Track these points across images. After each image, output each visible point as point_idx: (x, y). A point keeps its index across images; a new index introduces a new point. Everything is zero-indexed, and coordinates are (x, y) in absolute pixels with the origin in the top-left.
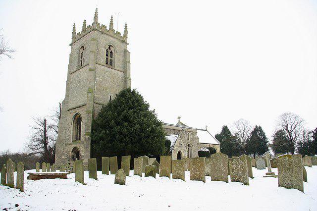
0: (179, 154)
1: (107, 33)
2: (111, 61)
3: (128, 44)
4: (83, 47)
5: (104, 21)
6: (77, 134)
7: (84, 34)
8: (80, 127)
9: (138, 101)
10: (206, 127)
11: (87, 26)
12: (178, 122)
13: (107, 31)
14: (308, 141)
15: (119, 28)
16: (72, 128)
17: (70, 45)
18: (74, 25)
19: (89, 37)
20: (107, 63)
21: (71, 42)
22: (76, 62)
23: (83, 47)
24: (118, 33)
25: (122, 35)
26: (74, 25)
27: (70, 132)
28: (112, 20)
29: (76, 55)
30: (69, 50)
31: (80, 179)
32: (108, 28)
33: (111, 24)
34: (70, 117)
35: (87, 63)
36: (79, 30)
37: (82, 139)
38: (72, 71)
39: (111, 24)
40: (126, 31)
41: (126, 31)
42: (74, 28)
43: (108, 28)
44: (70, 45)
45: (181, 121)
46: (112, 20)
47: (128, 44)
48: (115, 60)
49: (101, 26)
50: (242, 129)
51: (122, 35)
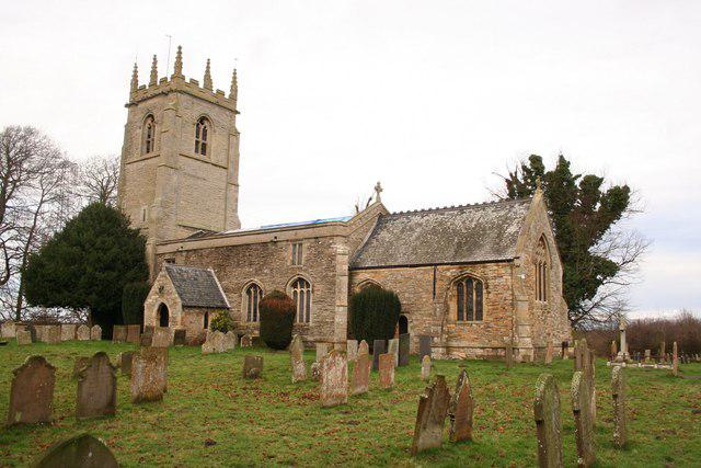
0: (163, 310)
2: (204, 145)
3: (237, 112)
4: (151, 116)
5: (193, 72)
10: (378, 189)
11: (159, 78)
14: (56, 233)
15: (221, 84)
17: (127, 106)
19: (170, 102)
20: (196, 151)
22: (139, 141)
30: (123, 115)
31: (563, 165)
32: (201, 86)
36: (144, 80)
39: (208, 77)
41: (234, 88)
44: (127, 106)
50: (426, 209)
51: (227, 96)
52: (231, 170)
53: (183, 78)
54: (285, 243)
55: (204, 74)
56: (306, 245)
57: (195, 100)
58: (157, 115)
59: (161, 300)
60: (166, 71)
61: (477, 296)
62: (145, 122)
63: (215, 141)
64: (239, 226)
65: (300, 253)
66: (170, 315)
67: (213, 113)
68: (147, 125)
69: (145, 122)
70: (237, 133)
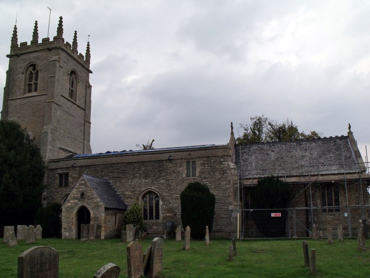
44: (8, 56)
52: (87, 111)
53: (63, 40)
54: (180, 161)
55: (73, 38)
56: (198, 162)
57: (69, 58)
58: (40, 66)
59: (80, 204)
60: (52, 35)
61: (335, 196)
62: (27, 70)
63: (80, 90)
64: (91, 152)
65: (194, 169)
66: (92, 215)
67: (79, 69)
68: (28, 72)
69: (27, 70)
70: (90, 87)
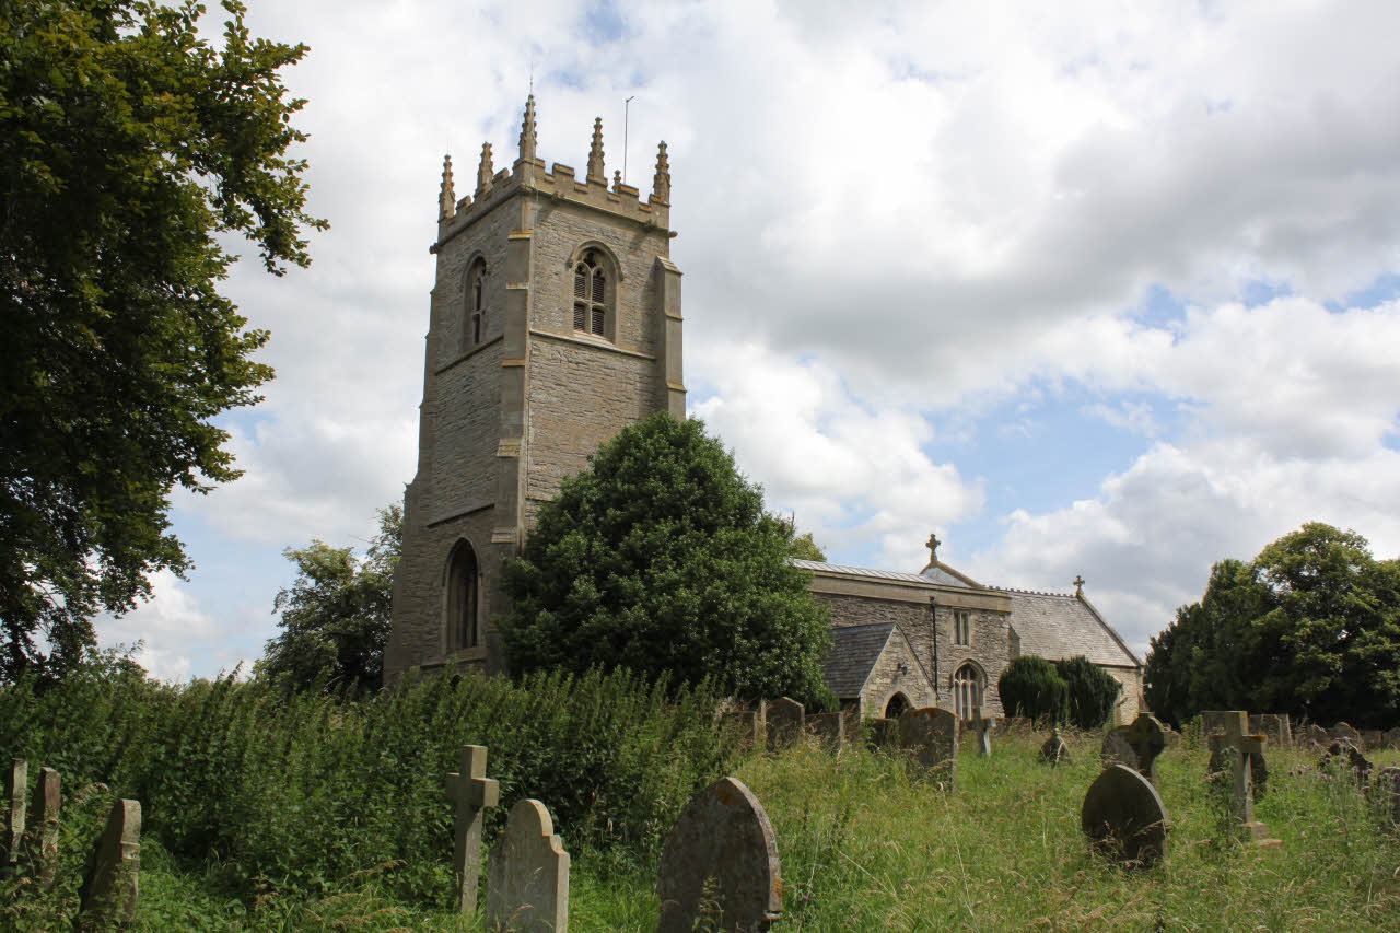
1: (581, 200)
3: (674, 235)
5: (562, 145)
6: (465, 622)
7: (484, 206)
8: (966, 627)
9: (698, 475)
12: (927, 561)
13: (579, 190)
15: (632, 167)
16: (445, 600)
17: (433, 250)
18: (447, 165)
21: (435, 240)
23: (479, 262)
24: (626, 192)
25: (644, 198)
26: (447, 165)
27: (438, 615)
28: (597, 136)
29: (456, 296)
32: (581, 176)
33: (596, 156)
34: (438, 555)
35: (498, 335)
36: (466, 187)
37: (479, 643)
38: (441, 366)
39: (596, 156)
40: (662, 179)
41: (662, 179)
42: (447, 175)
43: (581, 176)
44: (433, 250)
45: (940, 560)
46: (597, 136)
47: (674, 235)
48: (613, 308)
49: (549, 170)
51: (644, 198)
